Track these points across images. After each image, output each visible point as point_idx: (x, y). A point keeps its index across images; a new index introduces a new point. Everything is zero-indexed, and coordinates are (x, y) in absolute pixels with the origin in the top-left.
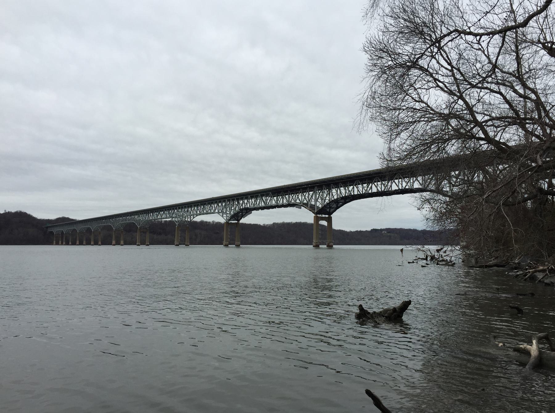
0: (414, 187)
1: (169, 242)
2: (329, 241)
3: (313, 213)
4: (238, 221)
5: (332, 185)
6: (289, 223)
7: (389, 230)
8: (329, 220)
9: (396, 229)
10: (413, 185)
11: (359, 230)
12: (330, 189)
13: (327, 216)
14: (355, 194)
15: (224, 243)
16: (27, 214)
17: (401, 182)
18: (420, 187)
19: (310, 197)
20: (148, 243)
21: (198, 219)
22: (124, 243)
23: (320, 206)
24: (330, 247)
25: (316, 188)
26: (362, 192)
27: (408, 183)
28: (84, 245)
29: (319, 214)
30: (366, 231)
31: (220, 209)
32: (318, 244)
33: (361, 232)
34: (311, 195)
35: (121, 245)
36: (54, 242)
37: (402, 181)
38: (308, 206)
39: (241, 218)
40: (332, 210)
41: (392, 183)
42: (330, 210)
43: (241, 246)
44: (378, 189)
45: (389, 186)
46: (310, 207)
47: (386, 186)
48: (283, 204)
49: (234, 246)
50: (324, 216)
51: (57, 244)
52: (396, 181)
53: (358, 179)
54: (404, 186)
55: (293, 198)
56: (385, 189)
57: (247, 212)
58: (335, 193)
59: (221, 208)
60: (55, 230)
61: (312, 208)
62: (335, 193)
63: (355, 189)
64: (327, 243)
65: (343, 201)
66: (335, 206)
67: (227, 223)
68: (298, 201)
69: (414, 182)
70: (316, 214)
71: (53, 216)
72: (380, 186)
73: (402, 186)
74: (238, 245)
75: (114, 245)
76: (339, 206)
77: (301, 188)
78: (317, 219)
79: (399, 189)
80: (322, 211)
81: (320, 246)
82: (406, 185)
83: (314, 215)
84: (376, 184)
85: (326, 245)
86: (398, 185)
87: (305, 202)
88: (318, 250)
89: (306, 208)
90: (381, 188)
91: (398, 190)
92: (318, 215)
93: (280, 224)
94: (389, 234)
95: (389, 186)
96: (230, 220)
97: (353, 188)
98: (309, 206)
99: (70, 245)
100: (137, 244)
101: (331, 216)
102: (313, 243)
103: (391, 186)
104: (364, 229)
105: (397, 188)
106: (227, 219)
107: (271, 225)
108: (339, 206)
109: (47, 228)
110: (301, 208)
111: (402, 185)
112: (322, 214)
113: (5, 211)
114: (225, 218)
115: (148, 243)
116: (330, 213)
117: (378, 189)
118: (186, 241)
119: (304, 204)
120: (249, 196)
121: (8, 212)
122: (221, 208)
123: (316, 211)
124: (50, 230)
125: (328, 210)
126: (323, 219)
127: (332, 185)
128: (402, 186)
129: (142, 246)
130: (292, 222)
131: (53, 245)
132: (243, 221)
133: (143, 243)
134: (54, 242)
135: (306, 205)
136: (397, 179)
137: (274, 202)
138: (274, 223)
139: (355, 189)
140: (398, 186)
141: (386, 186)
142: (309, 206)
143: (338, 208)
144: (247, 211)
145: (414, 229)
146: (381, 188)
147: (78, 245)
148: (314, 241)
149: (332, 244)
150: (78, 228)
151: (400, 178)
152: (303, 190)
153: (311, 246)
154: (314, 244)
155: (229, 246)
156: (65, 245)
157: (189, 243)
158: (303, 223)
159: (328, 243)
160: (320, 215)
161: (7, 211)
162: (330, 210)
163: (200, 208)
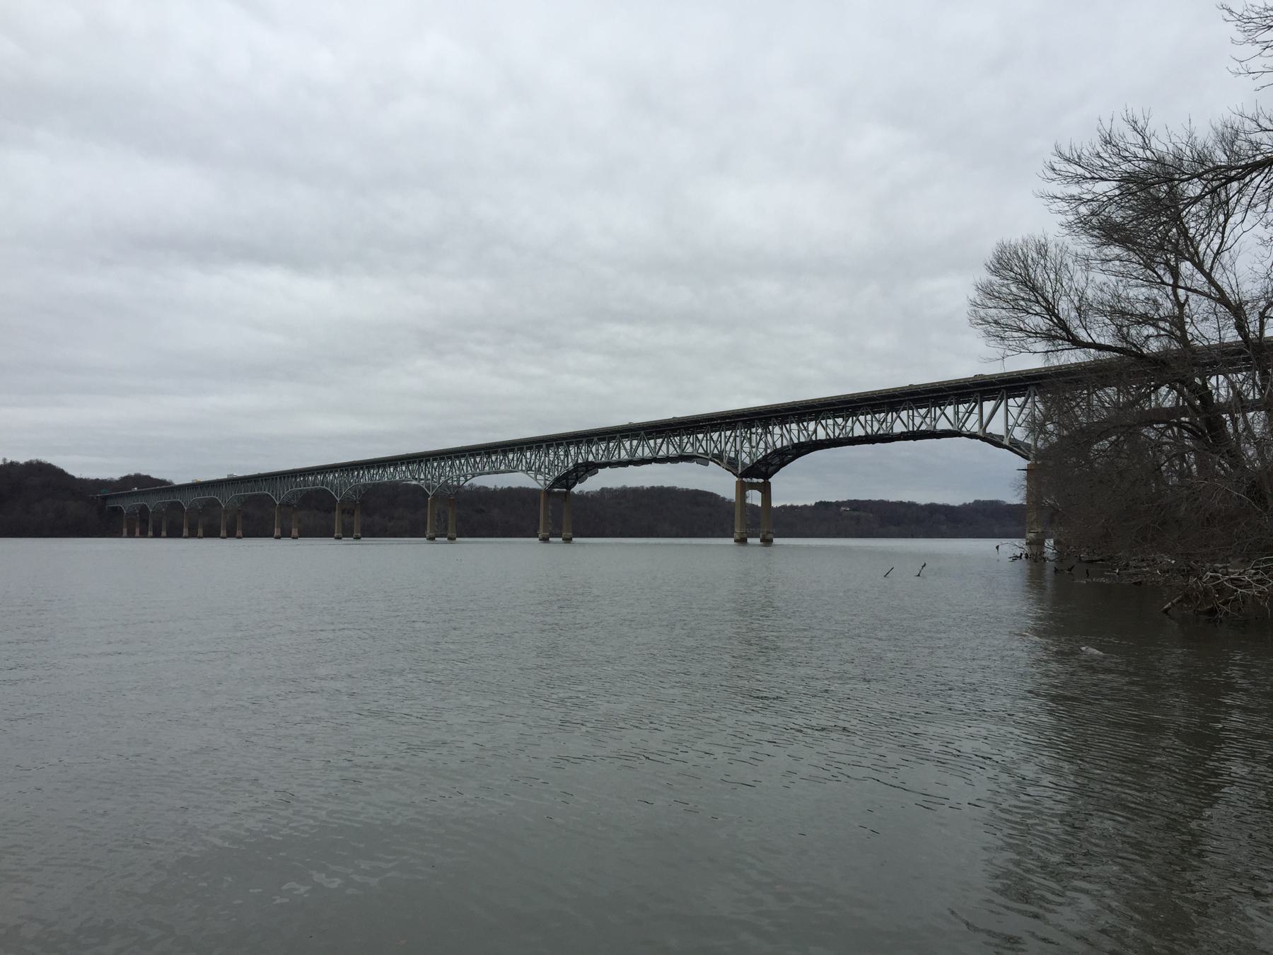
0: (855, 435)
1: (414, 530)
2: (766, 530)
3: (734, 474)
4: (569, 488)
5: (756, 421)
6: (637, 488)
7: (855, 505)
8: (766, 490)
9: (870, 501)
10: (892, 428)
11: (788, 504)
12: (765, 427)
13: (761, 481)
14: (801, 441)
15: (541, 533)
16: (17, 464)
17: (870, 423)
18: (950, 427)
19: (658, 448)
20: (359, 534)
21: (480, 481)
22: (298, 533)
23: (747, 461)
24: (767, 542)
25: (740, 424)
26: (799, 439)
27: (882, 424)
28: (200, 537)
29: (746, 478)
30: (805, 506)
31: (478, 467)
32: (745, 535)
33: (792, 508)
34: (659, 445)
35: (293, 538)
36: (125, 530)
37: (872, 420)
38: (722, 461)
39: (574, 484)
40: (771, 469)
41: (853, 423)
42: (767, 469)
43: (574, 539)
44: (827, 434)
45: (848, 429)
46: (729, 463)
47: (843, 428)
48: (668, 457)
49: (561, 539)
50: (755, 480)
51: (131, 535)
52: (862, 418)
53: (868, 405)
54: (875, 429)
55: (945, 417)
56: (840, 434)
57: (587, 471)
58: (779, 437)
59: (480, 465)
60: (126, 505)
61: (732, 465)
62: (779, 437)
63: (820, 429)
64: (761, 535)
65: (794, 451)
66: (777, 460)
67: (548, 492)
68: (701, 450)
69: (893, 422)
70: (741, 476)
71: (112, 471)
72: (832, 427)
73: (872, 430)
74: (569, 538)
75: (278, 538)
76: (785, 460)
77: (709, 425)
78: (742, 489)
79: (909, 432)
80: (751, 471)
81: (749, 540)
82: (922, 422)
83: (736, 479)
84: (823, 422)
85: (757, 536)
86: (906, 423)
87: (716, 451)
88: (742, 548)
89: (720, 465)
90: (834, 433)
91: (907, 432)
92: (744, 479)
93: (616, 490)
94: (856, 513)
95: (848, 429)
96: (552, 486)
97: (720, 435)
98: (725, 461)
99: (164, 537)
100: (336, 535)
101: (770, 480)
102: (735, 534)
103: (852, 429)
104: (799, 503)
105: (905, 430)
106: (545, 484)
107: (597, 493)
108: (785, 460)
109: (105, 498)
110: (707, 465)
111: (872, 427)
112: (751, 477)
113: (5, 460)
114: (542, 483)
115: (359, 534)
116: (767, 476)
117: (827, 434)
118: (449, 529)
119: (714, 456)
120: (596, 439)
121: (12, 463)
122: (480, 465)
123: (740, 472)
124: (111, 504)
125: (763, 469)
126: (753, 486)
127: (756, 421)
128: (872, 430)
129: (345, 540)
130: (642, 487)
131: (122, 537)
132: (577, 489)
133: (347, 532)
134: (125, 530)
135: (718, 458)
136: (863, 415)
137: (623, 454)
138: (603, 489)
139: (820, 429)
140: (864, 428)
141: (843, 428)
142: (725, 461)
143: (783, 464)
144: (590, 468)
145: (687, 489)
146: (834, 433)
147: (186, 537)
148: (737, 530)
149: (769, 536)
150: (186, 501)
151: (868, 413)
152: (711, 427)
153: (731, 541)
154: (737, 537)
155: (550, 539)
156: (152, 537)
157: (455, 535)
158: (668, 489)
159: (763, 536)
160: (749, 480)
161: (8, 461)
162: (767, 469)
163: (597, 450)
